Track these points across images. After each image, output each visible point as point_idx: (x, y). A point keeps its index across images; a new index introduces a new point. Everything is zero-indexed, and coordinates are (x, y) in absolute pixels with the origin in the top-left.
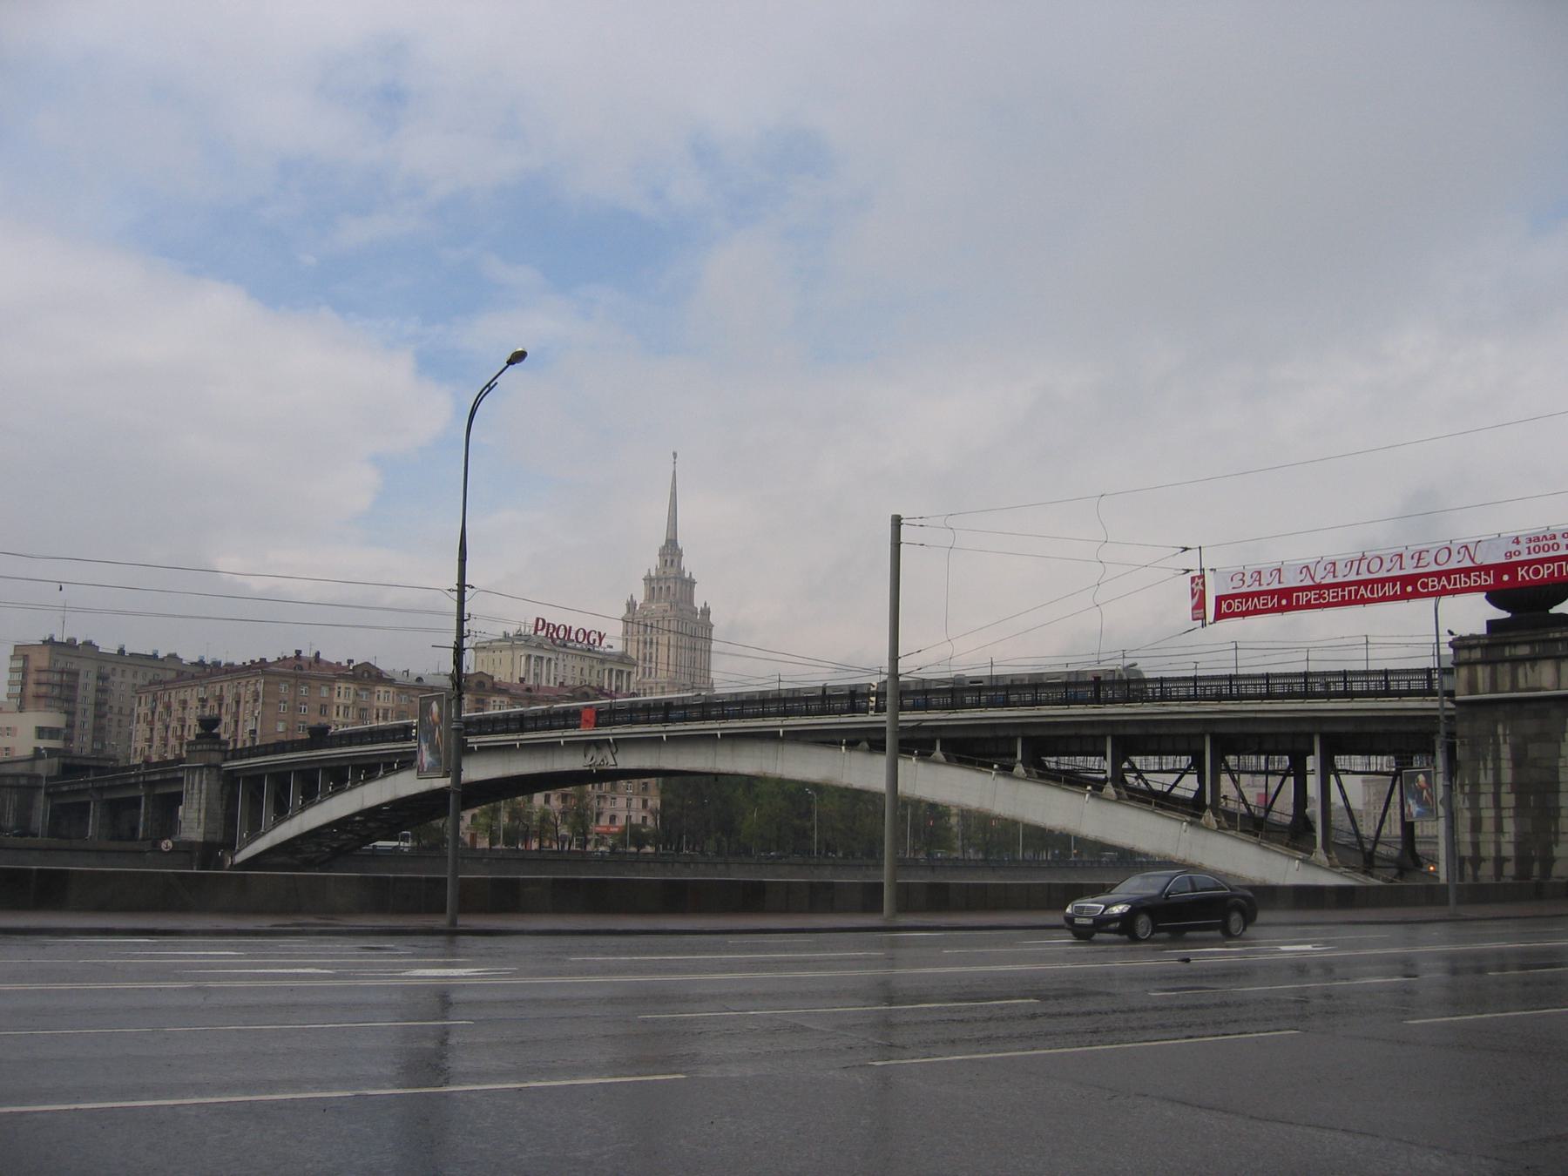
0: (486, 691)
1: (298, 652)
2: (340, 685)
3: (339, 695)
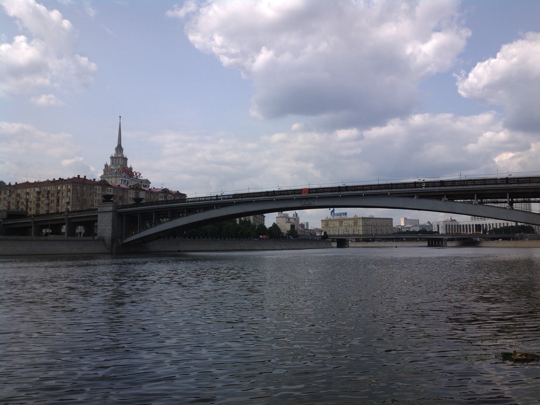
1: (79, 176)
2: (96, 187)
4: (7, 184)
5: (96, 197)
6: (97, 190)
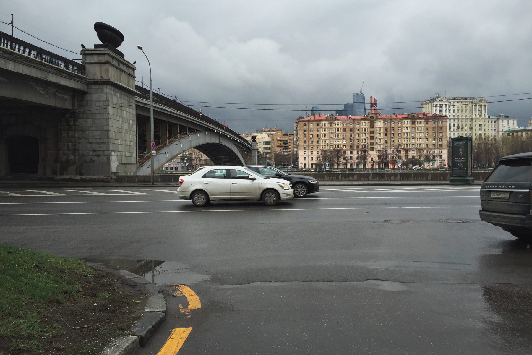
0: (374, 119)
2: (418, 120)
3: (362, 125)
6: (323, 125)
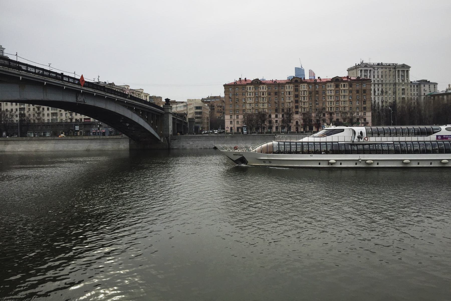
4: (220, 92)
5: (342, 93)
